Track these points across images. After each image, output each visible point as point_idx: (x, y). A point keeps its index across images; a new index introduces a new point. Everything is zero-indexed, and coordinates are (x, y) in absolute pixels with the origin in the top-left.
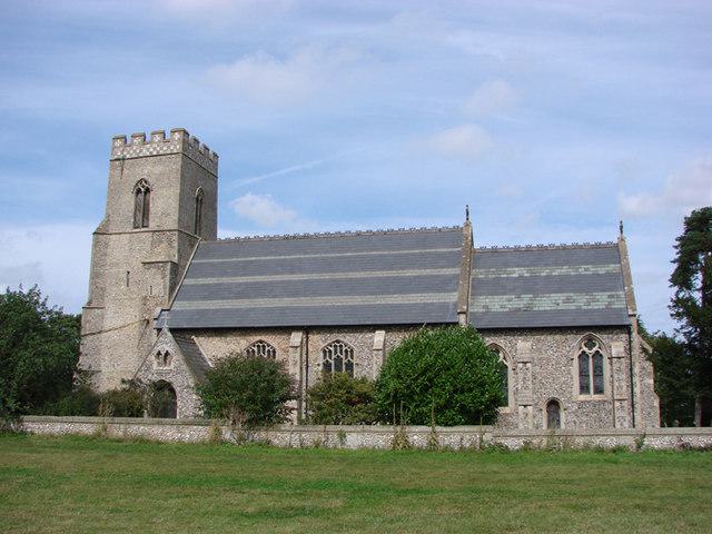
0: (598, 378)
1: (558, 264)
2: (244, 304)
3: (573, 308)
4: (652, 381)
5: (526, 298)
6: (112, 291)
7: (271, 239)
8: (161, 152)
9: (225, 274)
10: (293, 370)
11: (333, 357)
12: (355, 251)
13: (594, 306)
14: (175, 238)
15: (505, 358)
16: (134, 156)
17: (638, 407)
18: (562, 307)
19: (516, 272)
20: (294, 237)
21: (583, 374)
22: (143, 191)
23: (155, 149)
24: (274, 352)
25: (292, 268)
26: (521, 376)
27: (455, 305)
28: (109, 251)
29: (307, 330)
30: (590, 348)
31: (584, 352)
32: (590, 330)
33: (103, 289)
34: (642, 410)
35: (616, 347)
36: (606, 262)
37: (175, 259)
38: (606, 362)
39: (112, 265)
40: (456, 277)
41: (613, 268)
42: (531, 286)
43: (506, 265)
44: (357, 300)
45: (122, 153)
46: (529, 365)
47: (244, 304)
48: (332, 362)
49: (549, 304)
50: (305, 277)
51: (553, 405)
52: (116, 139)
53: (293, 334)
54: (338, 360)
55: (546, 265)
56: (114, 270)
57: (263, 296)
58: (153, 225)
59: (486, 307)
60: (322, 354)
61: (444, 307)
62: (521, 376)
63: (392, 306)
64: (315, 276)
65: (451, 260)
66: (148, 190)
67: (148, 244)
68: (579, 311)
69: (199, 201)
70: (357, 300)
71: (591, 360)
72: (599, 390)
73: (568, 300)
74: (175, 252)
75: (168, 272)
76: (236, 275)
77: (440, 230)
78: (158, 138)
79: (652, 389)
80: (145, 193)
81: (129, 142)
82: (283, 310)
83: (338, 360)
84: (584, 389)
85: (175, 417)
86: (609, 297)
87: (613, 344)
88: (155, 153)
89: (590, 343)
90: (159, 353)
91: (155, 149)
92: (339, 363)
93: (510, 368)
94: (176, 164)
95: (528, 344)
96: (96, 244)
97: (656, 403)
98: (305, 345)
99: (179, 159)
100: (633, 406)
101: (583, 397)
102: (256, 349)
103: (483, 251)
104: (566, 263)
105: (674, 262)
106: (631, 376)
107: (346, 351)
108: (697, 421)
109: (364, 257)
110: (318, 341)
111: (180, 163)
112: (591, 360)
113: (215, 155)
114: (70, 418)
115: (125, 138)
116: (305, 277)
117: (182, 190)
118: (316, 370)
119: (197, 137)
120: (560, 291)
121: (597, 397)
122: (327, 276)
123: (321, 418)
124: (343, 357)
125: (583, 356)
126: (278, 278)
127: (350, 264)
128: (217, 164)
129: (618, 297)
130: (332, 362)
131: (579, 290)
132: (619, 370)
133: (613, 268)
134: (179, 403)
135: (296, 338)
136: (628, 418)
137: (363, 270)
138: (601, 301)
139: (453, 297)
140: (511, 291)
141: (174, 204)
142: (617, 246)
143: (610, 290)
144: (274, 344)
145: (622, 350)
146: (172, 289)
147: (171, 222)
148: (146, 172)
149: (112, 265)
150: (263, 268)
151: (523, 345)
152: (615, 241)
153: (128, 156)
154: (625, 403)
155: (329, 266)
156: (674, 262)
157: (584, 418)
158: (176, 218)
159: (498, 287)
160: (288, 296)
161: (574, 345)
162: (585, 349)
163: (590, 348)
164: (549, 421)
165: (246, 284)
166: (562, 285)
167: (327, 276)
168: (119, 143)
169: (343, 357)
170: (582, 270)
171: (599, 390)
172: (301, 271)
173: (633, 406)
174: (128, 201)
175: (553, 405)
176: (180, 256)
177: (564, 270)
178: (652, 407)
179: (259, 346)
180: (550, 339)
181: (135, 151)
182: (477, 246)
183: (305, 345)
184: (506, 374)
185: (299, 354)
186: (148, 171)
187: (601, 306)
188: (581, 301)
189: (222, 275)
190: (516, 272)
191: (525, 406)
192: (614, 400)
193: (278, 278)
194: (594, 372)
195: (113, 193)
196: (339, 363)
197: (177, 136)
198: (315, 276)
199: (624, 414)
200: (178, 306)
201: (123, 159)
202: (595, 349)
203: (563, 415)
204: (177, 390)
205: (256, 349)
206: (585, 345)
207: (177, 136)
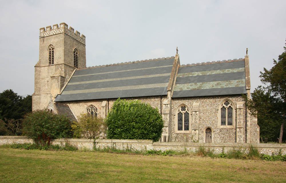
0: (230, 119)
1: (215, 69)
3: (220, 87)
4: (256, 120)
5: (199, 84)
8: (57, 33)
9: (83, 80)
11: (90, 111)
12: (132, 69)
14: (63, 67)
15: (188, 110)
16: (48, 35)
17: (248, 131)
19: (196, 74)
20: (110, 65)
21: (223, 116)
23: (54, 32)
24: (97, 109)
25: (107, 77)
26: (194, 117)
27: (167, 88)
28: (41, 73)
29: (108, 100)
30: (227, 105)
31: (180, 112)
32: (227, 96)
33: (40, 88)
34: (251, 133)
35: (240, 104)
36: (238, 67)
37: (63, 75)
38: (234, 111)
39: (42, 79)
40: (169, 76)
41: (241, 69)
42: (201, 79)
43: (192, 71)
44: (128, 88)
45: (43, 34)
46: (197, 113)
48: (90, 113)
49: (208, 86)
50: (111, 80)
51: (209, 130)
52: (41, 29)
53: (103, 102)
54: (92, 113)
55: (209, 70)
56: (43, 81)
57: (94, 88)
58: (55, 63)
59: (181, 89)
61: (162, 89)
63: (141, 89)
64: (114, 79)
65: (168, 70)
66: (53, 49)
67: (54, 69)
68: (222, 89)
70: (128, 88)
72: (230, 124)
73: (218, 84)
74: (63, 72)
75: (59, 80)
76: (86, 81)
77: (166, 59)
78: (55, 27)
79: (257, 123)
83: (92, 113)
84: (223, 123)
87: (238, 103)
88: (55, 34)
91: (54, 32)
92: (93, 114)
93: (190, 114)
94: (62, 37)
95: (198, 104)
96: (36, 70)
97: (258, 130)
99: (62, 36)
100: (246, 130)
101: (222, 127)
102: (90, 108)
104: (219, 69)
105: (265, 69)
107: (95, 109)
108: (280, 139)
110: (112, 103)
111: (63, 37)
116: (111, 80)
117: (65, 48)
119: (73, 27)
120: (215, 80)
121: (229, 127)
122: (119, 79)
123: (112, 135)
124: (94, 111)
125: (223, 109)
128: (85, 40)
132: (240, 114)
133: (241, 69)
135: (104, 103)
136: (244, 136)
138: (234, 84)
139: (166, 85)
140: (193, 82)
142: (244, 60)
144: (96, 106)
145: (242, 105)
147: (62, 61)
148: (52, 41)
149: (42, 79)
150: (97, 78)
151: (195, 104)
152: (244, 58)
153: (45, 36)
154: (242, 129)
155: (120, 75)
156: (265, 69)
157: (223, 136)
158: (63, 59)
159: (187, 80)
160: (103, 87)
161: (220, 103)
162: (225, 106)
163: (227, 105)
164: (206, 136)
166: (215, 78)
167: (119, 79)
168: (42, 31)
171: (230, 124)
172: (110, 78)
173: (246, 130)
174: (47, 54)
175: (209, 130)
177: (218, 72)
178: (256, 131)
179: (91, 107)
180: (208, 101)
184: (188, 117)
186: (53, 41)
187: (233, 86)
188: (224, 85)
190: (196, 74)
191: (195, 130)
192: (236, 128)
194: (228, 115)
195: (41, 50)
196: (93, 114)
197: (62, 26)
198: (114, 79)
199: (241, 134)
201: (44, 37)
202: (229, 105)
203: (213, 134)
205: (90, 108)
206: (225, 103)
207: (62, 26)
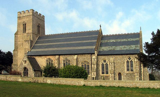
1: (123, 38)
2: (46, 49)
5: (113, 47)
6: (19, 47)
7: (61, 34)
10: (56, 65)
11: (66, 62)
12: (73, 37)
13: (131, 49)
18: (122, 49)
21: (128, 66)
22: (25, 25)
29: (59, 55)
30: (130, 60)
31: (128, 60)
36: (136, 38)
37: (32, 40)
39: (19, 41)
41: (137, 39)
43: (110, 39)
45: (20, 16)
47: (46, 49)
52: (18, 13)
58: (27, 32)
60: (63, 61)
61: (92, 49)
62: (111, 66)
63: (79, 49)
64: (63, 43)
65: (94, 38)
68: (127, 50)
69: (38, 27)
71: (130, 63)
73: (124, 47)
78: (27, 12)
80: (25, 25)
81: (29, 12)
82: (54, 51)
84: (128, 70)
85: (121, 80)
86: (135, 46)
88: (26, 15)
89: (130, 59)
90: (24, 61)
93: (109, 65)
96: (15, 36)
98: (59, 59)
101: (127, 72)
102: (48, 60)
103: (105, 36)
106: (141, 67)
109: (75, 38)
110: (62, 58)
112: (130, 63)
113: (43, 16)
114: (14, 75)
115: (20, 12)
118: (62, 66)
120: (123, 45)
121: (131, 72)
124: (68, 62)
125: (128, 62)
126: (55, 43)
127: (71, 40)
129: (138, 46)
130: (65, 63)
131: (127, 45)
133: (137, 39)
134: (29, 72)
137: (74, 41)
138: (133, 47)
140: (110, 45)
141: (31, 27)
143: (136, 44)
146: (31, 46)
147: (31, 31)
152: (139, 32)
155: (66, 40)
160: (56, 48)
162: (128, 60)
163: (130, 60)
165: (48, 45)
168: (19, 13)
169: (68, 62)
170: (129, 40)
171: (132, 70)
172: (60, 42)
176: (33, 39)
181: (22, 15)
182: (103, 34)
183: (59, 59)
184: (108, 66)
185: (57, 61)
186: (25, 20)
189: (42, 43)
193: (55, 43)
194: (131, 66)
195: (19, 25)
197: (31, 11)
198: (63, 43)
200: (32, 50)
202: (131, 60)
204: (28, 69)
205: (48, 60)
